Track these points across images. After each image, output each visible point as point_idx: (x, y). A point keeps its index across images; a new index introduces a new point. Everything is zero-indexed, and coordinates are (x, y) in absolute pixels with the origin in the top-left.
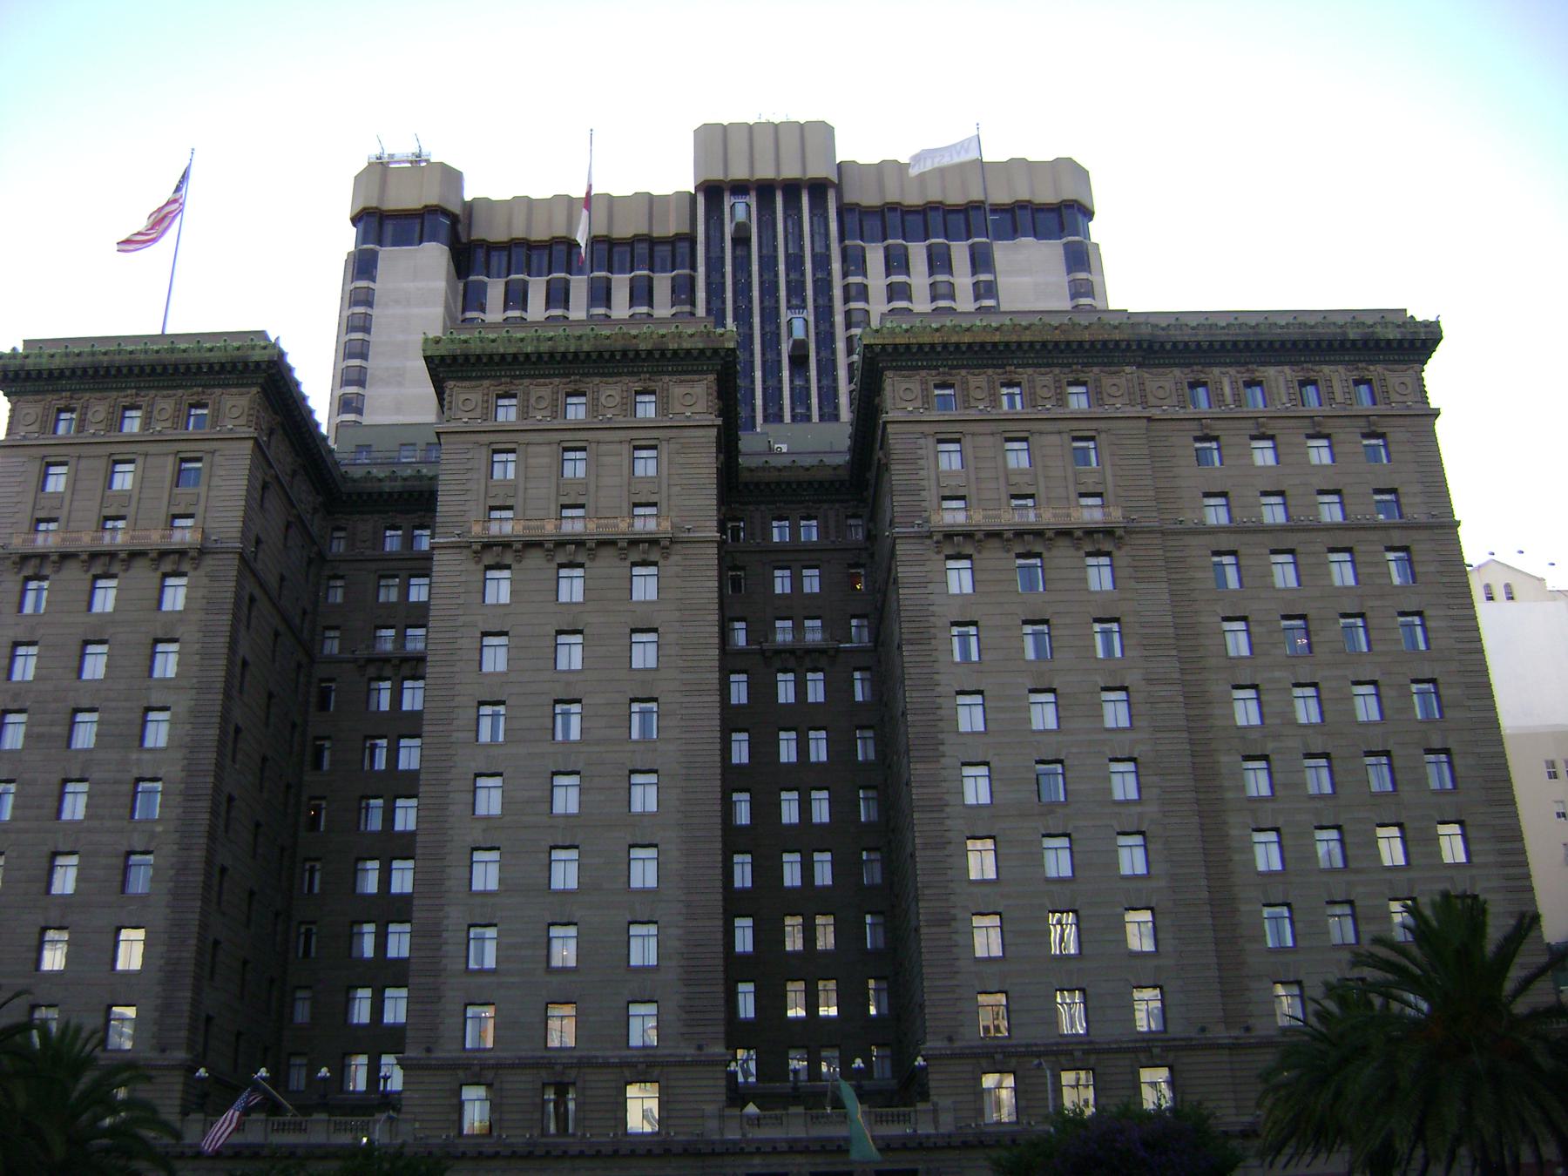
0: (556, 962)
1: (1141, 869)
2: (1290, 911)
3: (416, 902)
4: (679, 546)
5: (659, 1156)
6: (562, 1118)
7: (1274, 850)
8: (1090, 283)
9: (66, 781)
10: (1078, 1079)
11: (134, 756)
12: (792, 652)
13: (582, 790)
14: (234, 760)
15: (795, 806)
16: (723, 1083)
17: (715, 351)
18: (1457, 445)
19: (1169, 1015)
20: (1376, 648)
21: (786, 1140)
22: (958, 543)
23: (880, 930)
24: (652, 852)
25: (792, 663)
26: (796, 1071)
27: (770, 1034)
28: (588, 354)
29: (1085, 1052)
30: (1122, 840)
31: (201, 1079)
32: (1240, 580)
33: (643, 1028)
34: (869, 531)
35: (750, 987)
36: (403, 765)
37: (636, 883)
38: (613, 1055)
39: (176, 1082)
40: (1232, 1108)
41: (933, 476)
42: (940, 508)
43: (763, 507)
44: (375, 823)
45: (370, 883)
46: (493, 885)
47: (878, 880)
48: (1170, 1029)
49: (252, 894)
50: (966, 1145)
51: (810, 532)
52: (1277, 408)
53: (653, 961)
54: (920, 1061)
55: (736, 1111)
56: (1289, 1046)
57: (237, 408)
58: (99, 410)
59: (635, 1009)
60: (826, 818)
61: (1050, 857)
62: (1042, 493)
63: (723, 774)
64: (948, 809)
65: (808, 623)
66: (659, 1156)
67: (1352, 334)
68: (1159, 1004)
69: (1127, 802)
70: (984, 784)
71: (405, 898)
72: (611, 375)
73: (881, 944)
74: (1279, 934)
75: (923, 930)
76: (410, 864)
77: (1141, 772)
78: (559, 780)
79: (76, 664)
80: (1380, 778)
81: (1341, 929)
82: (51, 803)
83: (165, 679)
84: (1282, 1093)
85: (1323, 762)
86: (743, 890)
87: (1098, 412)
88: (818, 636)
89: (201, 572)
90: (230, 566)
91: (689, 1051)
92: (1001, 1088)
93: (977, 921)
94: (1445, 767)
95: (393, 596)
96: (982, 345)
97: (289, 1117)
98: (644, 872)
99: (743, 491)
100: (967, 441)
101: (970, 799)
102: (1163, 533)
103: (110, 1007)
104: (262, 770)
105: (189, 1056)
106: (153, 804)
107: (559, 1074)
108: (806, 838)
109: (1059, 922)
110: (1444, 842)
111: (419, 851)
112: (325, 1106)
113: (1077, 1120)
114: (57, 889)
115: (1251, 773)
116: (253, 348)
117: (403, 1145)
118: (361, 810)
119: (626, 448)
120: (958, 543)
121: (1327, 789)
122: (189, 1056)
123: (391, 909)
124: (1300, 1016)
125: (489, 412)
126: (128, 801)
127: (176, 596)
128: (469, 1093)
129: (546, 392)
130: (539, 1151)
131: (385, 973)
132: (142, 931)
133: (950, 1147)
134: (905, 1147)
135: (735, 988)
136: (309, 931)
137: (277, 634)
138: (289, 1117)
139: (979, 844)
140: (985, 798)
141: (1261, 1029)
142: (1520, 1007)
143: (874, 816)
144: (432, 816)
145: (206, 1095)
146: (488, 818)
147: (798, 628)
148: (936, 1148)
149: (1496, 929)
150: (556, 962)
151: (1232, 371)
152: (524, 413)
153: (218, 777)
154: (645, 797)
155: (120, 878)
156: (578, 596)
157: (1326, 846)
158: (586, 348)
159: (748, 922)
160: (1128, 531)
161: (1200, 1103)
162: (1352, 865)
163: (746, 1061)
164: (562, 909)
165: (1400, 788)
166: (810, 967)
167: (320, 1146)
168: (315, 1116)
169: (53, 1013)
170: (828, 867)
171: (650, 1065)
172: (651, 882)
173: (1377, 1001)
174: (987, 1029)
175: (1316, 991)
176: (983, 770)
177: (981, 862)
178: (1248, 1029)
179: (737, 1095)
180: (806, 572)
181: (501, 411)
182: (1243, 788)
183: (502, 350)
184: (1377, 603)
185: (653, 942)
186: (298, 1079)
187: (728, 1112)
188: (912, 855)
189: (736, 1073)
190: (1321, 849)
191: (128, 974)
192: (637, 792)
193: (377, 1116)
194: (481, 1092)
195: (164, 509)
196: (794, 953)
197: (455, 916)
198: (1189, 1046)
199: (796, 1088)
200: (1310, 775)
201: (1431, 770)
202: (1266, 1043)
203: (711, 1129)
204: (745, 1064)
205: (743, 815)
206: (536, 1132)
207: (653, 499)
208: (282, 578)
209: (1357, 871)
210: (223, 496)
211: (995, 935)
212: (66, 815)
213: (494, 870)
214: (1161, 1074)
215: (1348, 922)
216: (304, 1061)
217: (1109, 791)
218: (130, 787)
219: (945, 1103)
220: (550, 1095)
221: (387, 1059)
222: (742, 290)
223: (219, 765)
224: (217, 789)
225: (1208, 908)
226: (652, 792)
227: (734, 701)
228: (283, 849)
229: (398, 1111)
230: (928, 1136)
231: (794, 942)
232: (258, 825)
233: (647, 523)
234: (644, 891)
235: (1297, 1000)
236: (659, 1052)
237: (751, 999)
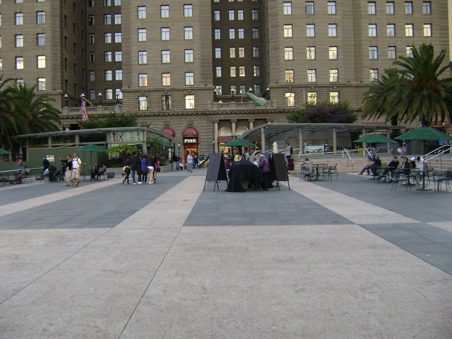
0: (164, 61)
1: (335, 35)
2: (377, 48)
3: (122, 45)
6: (168, 106)
7: (374, 30)
9: (16, 13)
10: (312, 95)
11: (35, 5)
13: (170, 11)
14: (65, 5)
15: (233, 15)
16: (213, 95)
19: (339, 77)
21: (230, 111)
23: (258, 52)
24: (191, 29)
26: (233, 92)
27: (225, 82)
29: (315, 87)
30: (330, 26)
31: (66, 97)
33: (190, 80)
35: (220, 68)
36: (116, 41)
37: (186, 38)
38: (181, 87)
39: (59, 99)
40: (355, 103)
44: (109, 22)
45: (109, 40)
46: (145, 39)
47: (257, 37)
48: (340, 81)
49: (75, 44)
50: (280, 112)
53: (192, 61)
54: (268, 89)
55: (216, 103)
56: (373, 88)
59: (187, 74)
60: (242, 19)
61: (308, 31)
63: (212, 5)
64: (278, 16)
68: (337, 75)
69: (332, 15)
70: (290, 8)
71: (120, 44)
73: (257, 18)
74: (373, 55)
75: (270, 52)
76: (120, 34)
77: (337, 5)
78: (163, 8)
80: (408, 10)
81: (391, 54)
82: (13, 20)
84: (369, 99)
85: (392, 4)
86: (218, 40)
91: (203, 86)
92: (291, 98)
93: (286, 49)
94: (429, 7)
97: (91, 107)
98: (189, 57)
101: (285, 13)
103: (38, 78)
104: (74, 8)
105: (62, 91)
106: (43, 19)
107: (166, 93)
108: (236, 25)
109: (310, 50)
110: (425, 30)
111: (122, 30)
112: (101, 104)
113: (312, 106)
114: (18, 45)
115: (370, 7)
117: (123, 113)
118: (104, 19)
121: (392, 13)
122: (62, 91)
123: (115, 47)
124: (377, 78)
126: (35, 18)
128: (141, 99)
130: (162, 114)
131: (116, 66)
132: (44, 57)
133: (275, 113)
134: (263, 113)
135: (216, 68)
136: (92, 36)
138: (91, 107)
139: (287, 27)
140: (290, 13)
141: (365, 82)
142: (440, 78)
143: (257, 18)
144: (125, 19)
145: (68, 102)
146: (142, 19)
148: (272, 113)
149: (436, 54)
150: (164, 61)
153: (61, 10)
155: (36, 42)
157: (390, 30)
159: (219, 49)
161: (346, 102)
162: (397, 36)
163: (219, 89)
164: (166, 46)
165: (414, 13)
166: (237, 62)
167: (101, 114)
168: (99, 106)
169: (22, 81)
170: (243, 33)
171: (192, 90)
172: (191, 38)
173: (400, 76)
174: (287, 81)
175: (382, 72)
176: (290, 4)
177: (288, 32)
178: (361, 82)
179: (216, 98)
182: (367, 11)
185: (192, 55)
186: (93, 96)
187: (214, 103)
188: (267, 30)
189: (216, 92)
190: (388, 31)
191: (42, 69)
192: (186, 11)
193: (116, 106)
194: (144, 98)
196: (233, 59)
197: (134, 49)
198: (344, 86)
199: (233, 96)
200: (387, 8)
201: (424, 8)
202: (366, 86)
204: (219, 90)
205: (218, 18)
206: (161, 109)
209: (399, 37)
211: (291, 53)
212: (18, 24)
213: (145, 35)
214: (336, 94)
215: (394, 52)
216: (94, 91)
217: (327, 11)
218: (35, 14)
219: (275, 100)
220: (164, 98)
221: (117, 90)
223: (61, 6)
224: (61, 14)
225: (353, 47)
226: (191, 11)
227: (216, 38)
228: (83, 31)
229: (122, 104)
230: (270, 110)
231: (232, 55)
232: (74, 24)
234: (189, 40)
235: (376, 74)
236: (194, 86)
237: (220, 71)
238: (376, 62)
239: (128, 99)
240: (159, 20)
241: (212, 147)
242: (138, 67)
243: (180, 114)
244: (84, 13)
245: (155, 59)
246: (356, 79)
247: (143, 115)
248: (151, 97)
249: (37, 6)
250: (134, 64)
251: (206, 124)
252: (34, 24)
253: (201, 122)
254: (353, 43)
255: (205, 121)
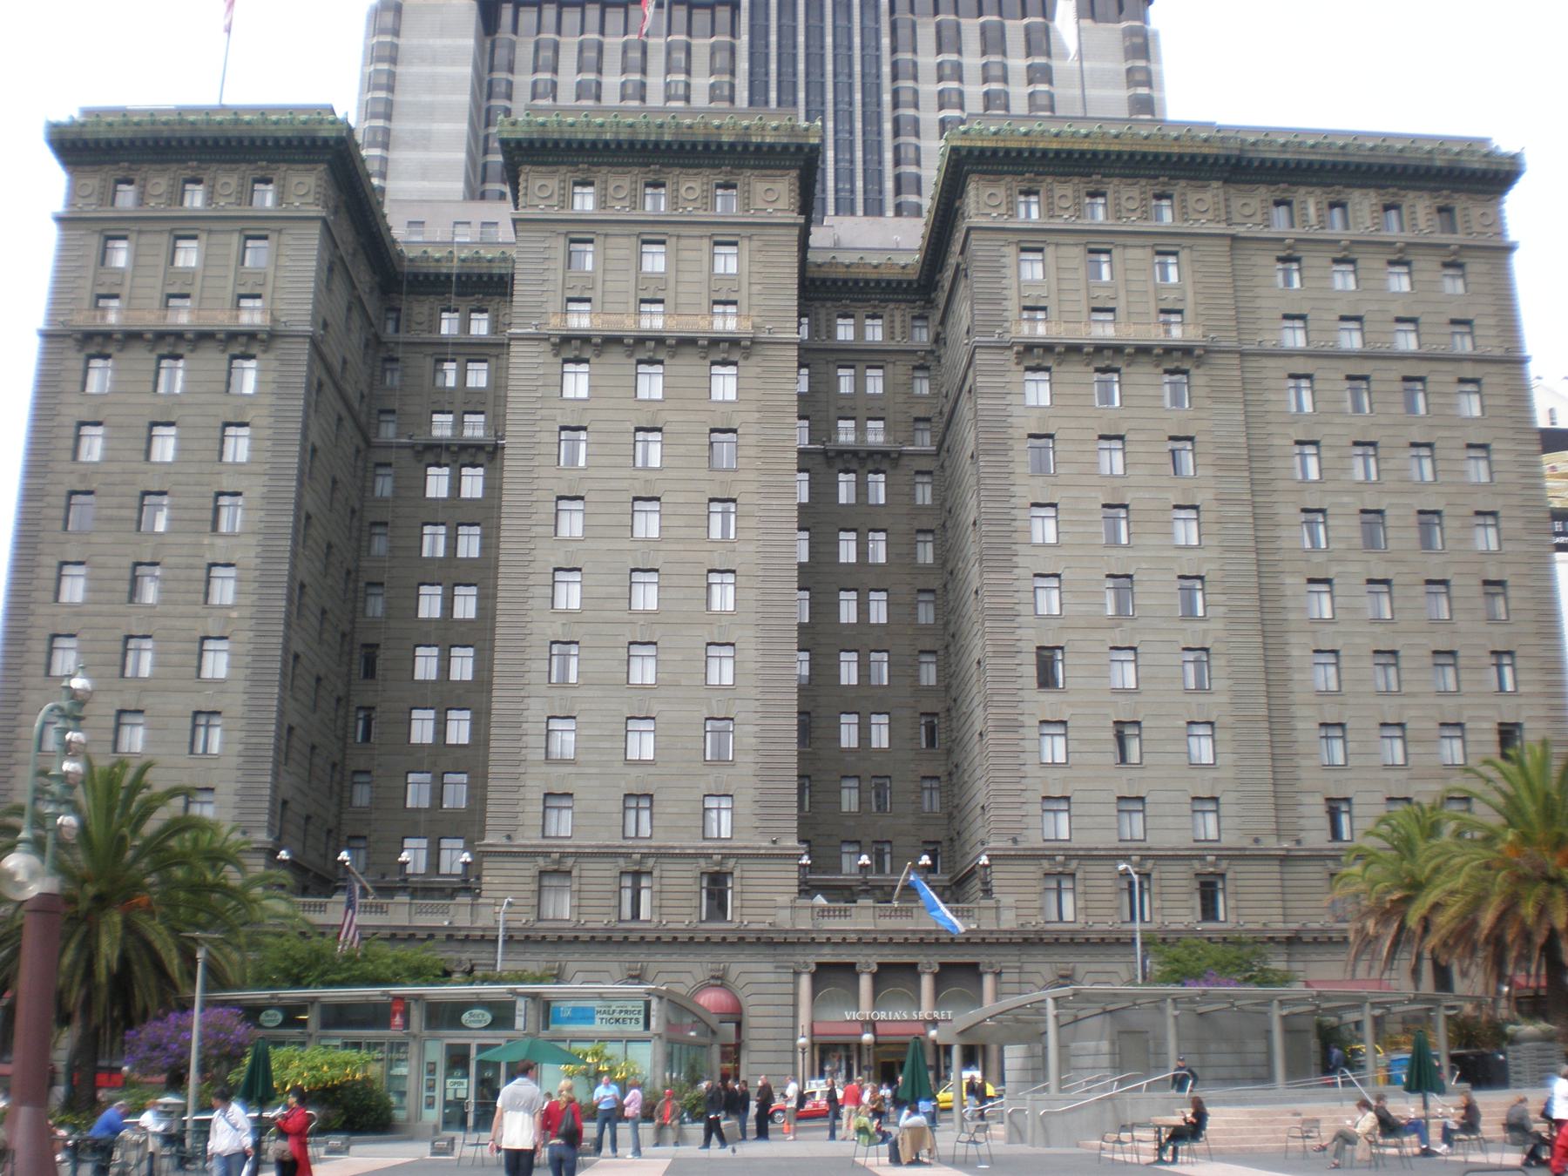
4: (759, 348)
5: (732, 944)
8: (1148, 72)
12: (855, 453)
16: (796, 875)
17: (799, 147)
18: (1527, 274)
20: (1441, 478)
22: (1037, 356)
25: (854, 466)
28: (669, 144)
32: (1314, 403)
34: (938, 334)
41: (1015, 285)
42: (1021, 319)
43: (829, 304)
49: (319, 679)
51: (875, 333)
52: (1355, 233)
57: (305, 190)
58: (160, 183)
62: (1121, 305)
64: (1019, 619)
65: (871, 424)
66: (732, 944)
67: (1439, 162)
72: (691, 167)
79: (143, 446)
83: (235, 464)
87: (1185, 227)
88: (881, 438)
89: (270, 356)
90: (302, 351)
95: (451, 381)
96: (1070, 153)
99: (823, 290)
100: (1049, 250)
102: (1243, 354)
116: (321, 122)
119: (706, 243)
120: (1037, 356)
125: (566, 201)
127: (249, 378)
129: (626, 182)
133: (1010, 943)
137: (340, 419)
146: (568, 612)
147: (861, 430)
148: (998, 943)
151: (1318, 191)
152: (602, 203)
153: (293, 566)
154: (724, 597)
156: (658, 394)
158: (667, 138)
160: (1207, 351)
162: (1404, 689)
180: (869, 372)
181: (577, 199)
183: (580, 136)
184: (1447, 434)
187: (800, 902)
195: (230, 289)
203: (784, 919)
207: (733, 297)
208: (345, 362)
210: (282, 273)
218: (202, 574)
219: (1006, 900)
222: (843, 88)
223: (294, 554)
224: (292, 577)
230: (991, 932)
233: (727, 323)
238: (1338, 775)
239: (503, 880)
240: (626, 616)
241: (789, 1057)
242: (545, 769)
243: (683, 937)
244: (353, 575)
245: (602, 745)
246: (1279, 834)
247: (551, 936)
248: (585, 873)
249: (212, 545)
250: (530, 757)
251: (772, 978)
252: (195, 603)
253: (753, 967)
254: (1264, 712)
255: (770, 967)
